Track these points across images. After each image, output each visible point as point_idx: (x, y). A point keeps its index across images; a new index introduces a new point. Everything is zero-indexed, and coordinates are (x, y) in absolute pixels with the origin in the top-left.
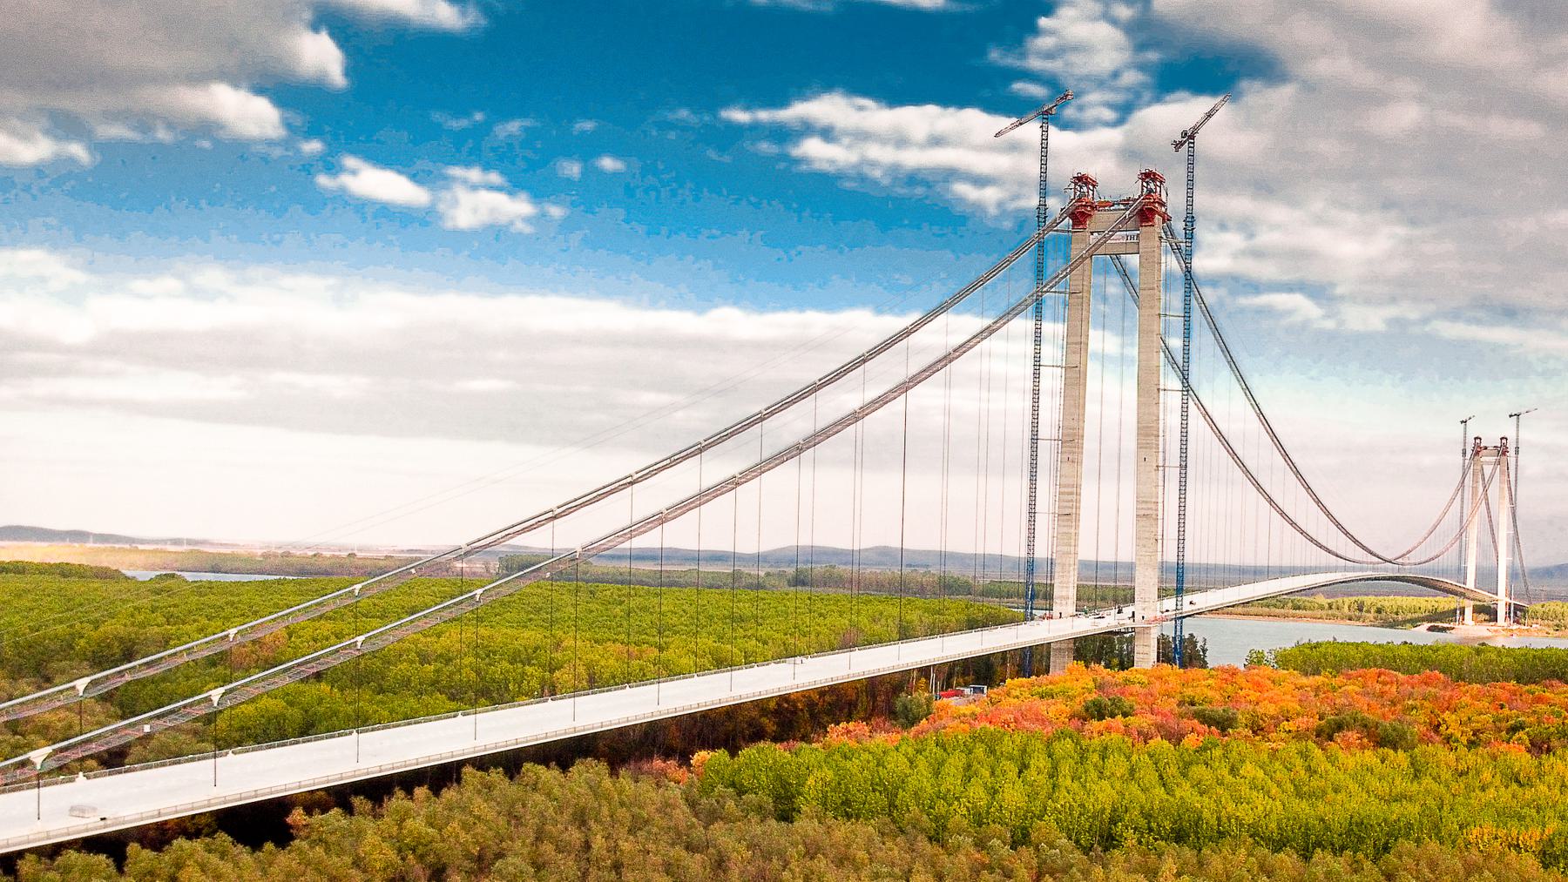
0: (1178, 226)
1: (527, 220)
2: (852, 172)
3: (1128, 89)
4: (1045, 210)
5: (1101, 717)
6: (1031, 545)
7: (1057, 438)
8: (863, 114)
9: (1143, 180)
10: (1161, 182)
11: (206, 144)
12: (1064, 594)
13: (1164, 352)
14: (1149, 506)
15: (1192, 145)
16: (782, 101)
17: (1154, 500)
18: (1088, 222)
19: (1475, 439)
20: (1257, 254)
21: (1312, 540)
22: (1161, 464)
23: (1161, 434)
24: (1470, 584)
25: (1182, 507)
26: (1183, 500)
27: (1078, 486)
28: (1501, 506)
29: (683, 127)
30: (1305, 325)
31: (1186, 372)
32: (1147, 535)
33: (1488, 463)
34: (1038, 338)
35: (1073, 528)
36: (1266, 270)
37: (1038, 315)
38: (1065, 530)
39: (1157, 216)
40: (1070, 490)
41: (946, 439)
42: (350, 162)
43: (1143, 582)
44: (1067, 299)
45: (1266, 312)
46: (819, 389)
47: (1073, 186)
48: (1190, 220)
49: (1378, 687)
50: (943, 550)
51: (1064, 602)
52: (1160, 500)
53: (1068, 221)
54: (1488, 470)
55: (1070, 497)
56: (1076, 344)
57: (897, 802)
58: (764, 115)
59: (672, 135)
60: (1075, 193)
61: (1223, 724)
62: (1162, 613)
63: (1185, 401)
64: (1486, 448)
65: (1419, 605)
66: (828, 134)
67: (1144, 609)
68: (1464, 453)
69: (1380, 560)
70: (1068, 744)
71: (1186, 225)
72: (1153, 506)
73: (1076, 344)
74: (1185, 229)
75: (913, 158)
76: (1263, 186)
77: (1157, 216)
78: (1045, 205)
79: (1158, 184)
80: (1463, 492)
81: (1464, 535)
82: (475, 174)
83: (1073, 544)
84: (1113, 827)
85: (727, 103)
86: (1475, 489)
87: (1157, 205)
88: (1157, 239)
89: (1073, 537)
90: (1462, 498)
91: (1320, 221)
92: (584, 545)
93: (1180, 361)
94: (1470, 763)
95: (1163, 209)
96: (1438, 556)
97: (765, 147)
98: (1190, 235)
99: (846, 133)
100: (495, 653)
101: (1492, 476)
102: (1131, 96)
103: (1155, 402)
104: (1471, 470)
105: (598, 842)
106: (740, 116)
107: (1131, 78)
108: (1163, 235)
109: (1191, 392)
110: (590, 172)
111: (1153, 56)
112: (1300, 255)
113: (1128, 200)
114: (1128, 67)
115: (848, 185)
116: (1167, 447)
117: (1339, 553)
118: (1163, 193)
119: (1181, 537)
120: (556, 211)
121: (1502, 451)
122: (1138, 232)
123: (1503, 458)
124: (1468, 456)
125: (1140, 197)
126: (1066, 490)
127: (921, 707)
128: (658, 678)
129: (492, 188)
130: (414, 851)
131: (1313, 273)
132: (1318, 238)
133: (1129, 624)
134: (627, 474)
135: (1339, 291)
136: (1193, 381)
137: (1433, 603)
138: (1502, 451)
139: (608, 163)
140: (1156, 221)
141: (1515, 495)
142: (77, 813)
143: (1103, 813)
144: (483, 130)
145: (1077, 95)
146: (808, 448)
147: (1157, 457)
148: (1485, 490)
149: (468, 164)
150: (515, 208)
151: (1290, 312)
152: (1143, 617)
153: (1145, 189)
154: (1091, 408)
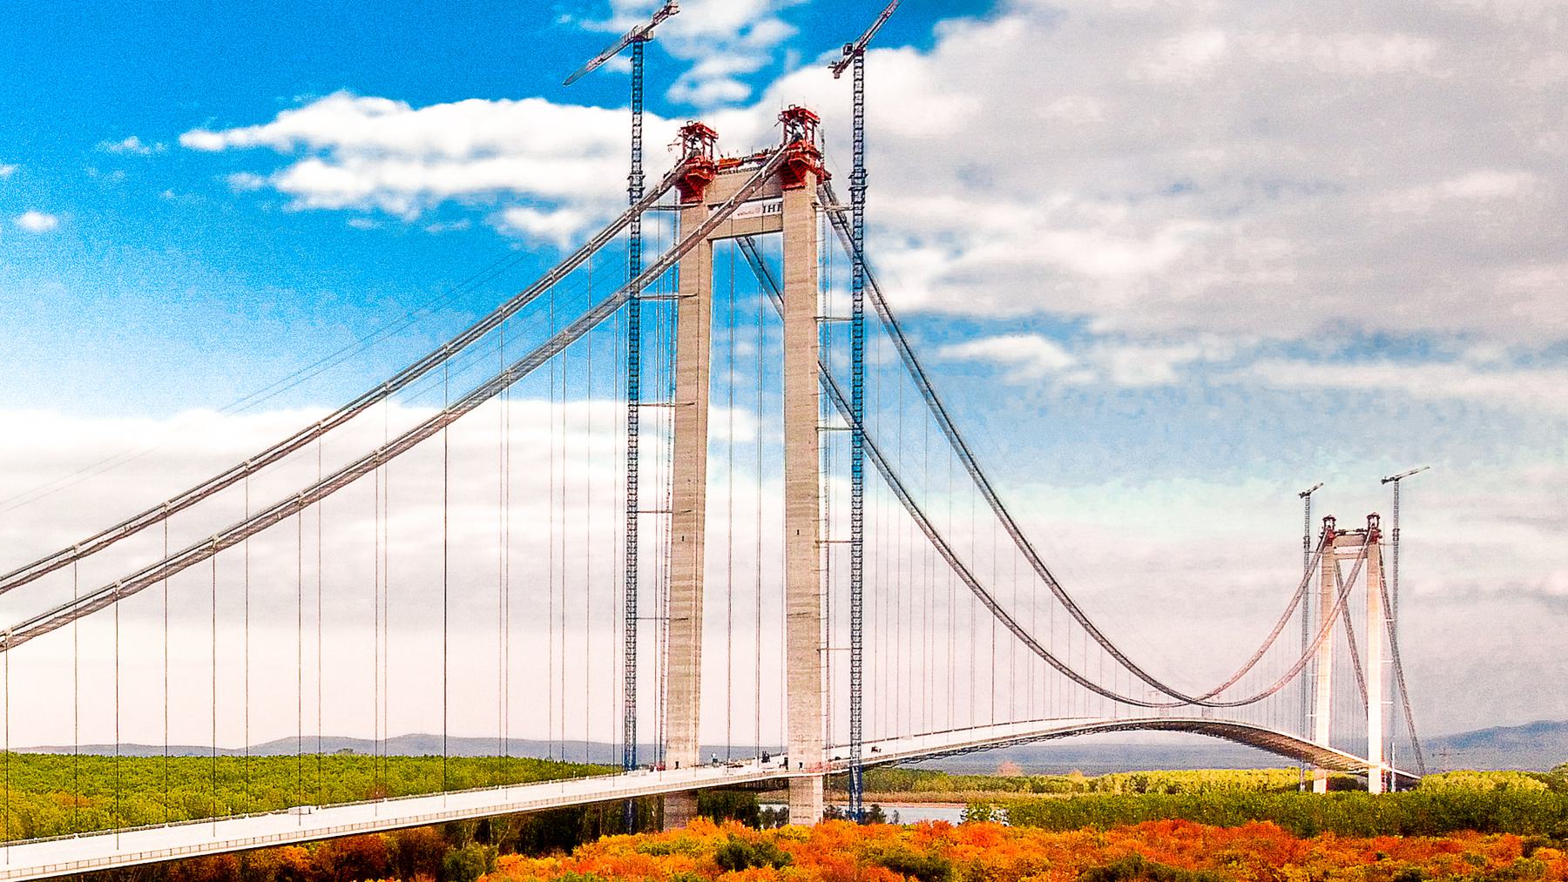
2: (366, 207)
4: (641, 179)
5: (740, 867)
6: (630, 723)
7: (664, 509)
8: (376, 121)
9: (786, 122)
12: (681, 734)
13: (824, 383)
14: (805, 600)
15: (860, 64)
16: (266, 116)
17: (813, 591)
18: (704, 192)
19: (1325, 519)
21: (1060, 667)
22: (822, 537)
26: (858, 615)
27: (699, 578)
28: (1370, 606)
29: (129, 161)
30: (1048, 380)
31: (859, 243)
33: (1348, 556)
34: (634, 426)
35: (693, 638)
36: (983, 304)
38: (681, 641)
39: (809, 173)
40: (686, 583)
43: (800, 712)
44: (679, 216)
45: (982, 369)
46: (324, 432)
47: (681, 140)
49: (1174, 841)
50: (503, 736)
51: (682, 746)
52: (823, 590)
54: (1347, 567)
55: (688, 594)
58: (241, 137)
59: (119, 175)
60: (685, 152)
62: (830, 761)
64: (1343, 533)
65: (1236, 780)
67: (802, 753)
68: (1307, 543)
71: (853, 183)
72: (813, 601)
73: (690, 370)
74: (851, 189)
75: (451, 180)
77: (809, 173)
78: (641, 172)
79: (810, 125)
80: (1306, 603)
81: (1309, 663)
83: (693, 716)
85: (187, 126)
86: (1325, 596)
87: (808, 156)
89: (693, 652)
91: (1061, 222)
93: (847, 394)
95: (818, 163)
97: (254, 182)
98: (858, 396)
102: (769, 60)
103: (811, 447)
106: (204, 140)
107: (772, 31)
108: (818, 201)
112: (1032, 273)
113: (765, 153)
114: (765, 16)
116: (832, 710)
117: (1105, 687)
121: (1371, 536)
122: (780, 200)
124: (1314, 545)
125: (781, 147)
126: (681, 583)
128: (117, 827)
132: (1067, 248)
133: (780, 773)
134: (69, 546)
135: (1098, 326)
136: (868, 424)
137: (1260, 777)
138: (1371, 536)
141: (1396, 596)
145: (689, 64)
146: (310, 503)
148: (1343, 598)
151: (1021, 364)
152: (801, 764)
153: (790, 136)
154: (714, 525)
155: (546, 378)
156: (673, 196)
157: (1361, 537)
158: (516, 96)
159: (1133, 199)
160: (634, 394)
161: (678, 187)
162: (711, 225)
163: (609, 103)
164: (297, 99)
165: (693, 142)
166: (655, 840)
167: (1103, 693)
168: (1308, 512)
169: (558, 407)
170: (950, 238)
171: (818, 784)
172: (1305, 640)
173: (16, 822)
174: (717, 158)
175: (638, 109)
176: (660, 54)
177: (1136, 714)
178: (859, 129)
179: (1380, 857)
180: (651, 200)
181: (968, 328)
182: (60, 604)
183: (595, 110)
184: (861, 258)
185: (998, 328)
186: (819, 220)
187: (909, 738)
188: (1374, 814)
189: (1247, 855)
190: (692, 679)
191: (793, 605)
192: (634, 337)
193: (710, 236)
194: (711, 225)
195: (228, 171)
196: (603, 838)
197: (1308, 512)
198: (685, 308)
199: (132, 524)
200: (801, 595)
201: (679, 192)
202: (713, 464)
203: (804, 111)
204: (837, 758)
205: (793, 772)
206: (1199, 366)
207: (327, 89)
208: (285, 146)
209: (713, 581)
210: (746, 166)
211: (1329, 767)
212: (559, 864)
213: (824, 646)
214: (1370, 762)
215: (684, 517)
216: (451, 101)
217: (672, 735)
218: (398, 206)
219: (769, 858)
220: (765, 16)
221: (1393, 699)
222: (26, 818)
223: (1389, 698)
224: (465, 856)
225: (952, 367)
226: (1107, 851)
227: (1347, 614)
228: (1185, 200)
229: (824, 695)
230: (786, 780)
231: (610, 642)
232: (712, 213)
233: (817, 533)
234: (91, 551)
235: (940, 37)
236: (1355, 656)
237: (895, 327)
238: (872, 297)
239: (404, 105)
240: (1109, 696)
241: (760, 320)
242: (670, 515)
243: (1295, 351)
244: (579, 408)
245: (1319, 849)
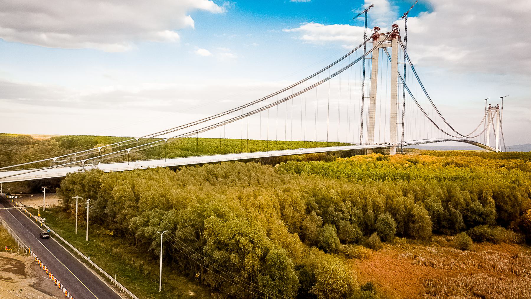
0: (403, 39)
7: (370, 77)
9: (393, 27)
10: (398, 27)
12: (371, 138)
16: (298, 27)
23: (398, 95)
24: (488, 145)
25: (403, 130)
31: (405, 81)
32: (394, 122)
37: (366, 27)
38: (371, 121)
39: (397, 36)
40: (373, 111)
48: (406, 37)
51: (371, 141)
53: (372, 40)
54: (493, 113)
55: (372, 113)
56: (374, 72)
58: (293, 30)
63: (404, 102)
64: (492, 107)
66: (309, 34)
69: (461, 136)
72: (395, 114)
73: (374, 72)
77: (397, 36)
86: (489, 119)
93: (403, 78)
94: (488, 171)
95: (398, 35)
100: (228, 146)
105: (253, 174)
109: (406, 87)
118: (399, 30)
119: (403, 132)
121: (498, 108)
130: (210, 174)
138: (498, 108)
140: (396, 37)
142: (136, 165)
153: (393, 29)
238: (408, 60)
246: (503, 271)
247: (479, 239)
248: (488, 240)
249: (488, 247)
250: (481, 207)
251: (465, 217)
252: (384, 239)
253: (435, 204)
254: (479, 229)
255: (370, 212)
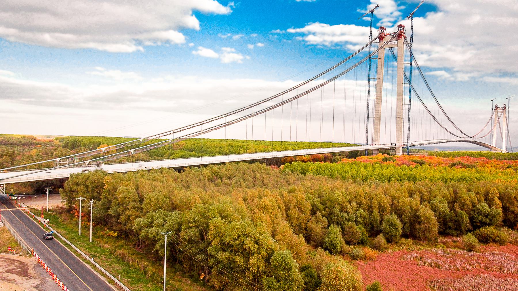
0: (408, 39)
1: (241, 60)
2: (321, 44)
3: (396, 17)
4: (372, 37)
5: (386, 161)
9: (399, 27)
11: (168, 45)
12: (376, 139)
16: (303, 26)
17: (401, 113)
20: (431, 60)
22: (403, 103)
27: (381, 110)
33: (500, 112)
34: (369, 86)
38: (377, 122)
39: (403, 37)
40: (378, 111)
41: (344, 114)
42: (200, 48)
45: (433, 76)
48: (412, 36)
51: (376, 141)
52: (403, 113)
54: (499, 114)
57: (333, 173)
58: (298, 30)
61: (421, 164)
64: (499, 108)
68: (492, 109)
70: (378, 165)
72: (401, 115)
75: (337, 39)
76: (434, 41)
77: (403, 37)
80: (492, 120)
81: (492, 131)
82: (229, 49)
84: (390, 179)
85: (289, 27)
86: (495, 119)
87: (402, 33)
88: (403, 43)
90: (492, 122)
91: (449, 50)
92: (255, 112)
93: (409, 79)
95: (404, 35)
96: (483, 137)
97: (300, 38)
99: (319, 34)
101: (501, 115)
102: (395, 19)
104: (494, 114)
107: (397, 14)
110: (256, 47)
111: (402, 7)
114: (396, 11)
115: (319, 47)
120: (248, 57)
121: (504, 108)
123: (504, 110)
124: (493, 110)
126: (377, 111)
127: (339, 159)
129: (233, 52)
130: (214, 174)
131: (448, 66)
133: (394, 146)
135: (455, 69)
138: (504, 108)
139: (260, 45)
141: (508, 121)
143: (387, 176)
144: (230, 38)
145: (381, 19)
147: (402, 102)
149: (227, 47)
150: (238, 57)
151: (441, 76)
154: (383, 104)
155: (353, 74)
156: (377, 40)
157: (502, 109)
158: (349, 24)
159: (462, 46)
160: (369, 80)
161: (379, 38)
162: (384, 46)
163: (366, 26)
164: (309, 23)
165: (382, 30)
166: (371, 157)
167: (454, 135)
168: (493, 104)
169: (355, 82)
170: (429, 53)
171: (401, 149)
172: (491, 127)
173: (254, 150)
174: (386, 33)
175: (371, 27)
176: (375, 17)
177: (460, 139)
178: (412, 33)
179: (504, 163)
180: (373, 41)
181: (430, 69)
182: (263, 109)
183: (364, 27)
184: (412, 52)
185: (436, 69)
186: (404, 45)
187: (418, 142)
188: (503, 156)
189: (480, 162)
190: (379, 129)
191: (398, 116)
192: (370, 65)
193: (384, 47)
194: (384, 46)
195: (296, 36)
196: (361, 156)
197: (493, 104)
198: (379, 60)
199: (277, 96)
200: (399, 114)
201: (379, 40)
202: (383, 93)
203: (402, 25)
204: (405, 144)
205: (397, 146)
206: (473, 78)
207: (314, 22)
208: (307, 32)
209: (383, 114)
210: (391, 35)
211: (495, 150)
212: (353, 160)
213: (403, 123)
214: (503, 150)
215: (378, 99)
216: (337, 25)
217: (375, 139)
218: (327, 44)
219: (392, 160)
220: (396, 11)
221: (507, 138)
222: (255, 149)
223: (507, 138)
224: (336, 158)
225: (429, 76)
226: (454, 161)
227: (499, 123)
228: (472, 46)
229: (403, 132)
230: (395, 148)
231: (363, 125)
232: (384, 43)
233: (402, 102)
234: (269, 100)
235: (427, 16)
236: (501, 130)
237: (419, 68)
239: (329, 25)
240: (455, 136)
241: (393, 66)
242: (375, 99)
243: (492, 75)
244: (359, 82)
245: (490, 259)
246: (509, 273)
247: (485, 240)
248: (494, 241)
249: (495, 248)
250: (487, 208)
251: (471, 219)
252: (389, 240)
253: (441, 205)
254: (485, 230)
255: (376, 213)
